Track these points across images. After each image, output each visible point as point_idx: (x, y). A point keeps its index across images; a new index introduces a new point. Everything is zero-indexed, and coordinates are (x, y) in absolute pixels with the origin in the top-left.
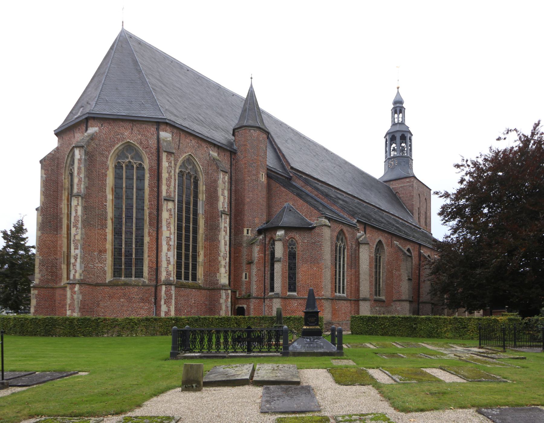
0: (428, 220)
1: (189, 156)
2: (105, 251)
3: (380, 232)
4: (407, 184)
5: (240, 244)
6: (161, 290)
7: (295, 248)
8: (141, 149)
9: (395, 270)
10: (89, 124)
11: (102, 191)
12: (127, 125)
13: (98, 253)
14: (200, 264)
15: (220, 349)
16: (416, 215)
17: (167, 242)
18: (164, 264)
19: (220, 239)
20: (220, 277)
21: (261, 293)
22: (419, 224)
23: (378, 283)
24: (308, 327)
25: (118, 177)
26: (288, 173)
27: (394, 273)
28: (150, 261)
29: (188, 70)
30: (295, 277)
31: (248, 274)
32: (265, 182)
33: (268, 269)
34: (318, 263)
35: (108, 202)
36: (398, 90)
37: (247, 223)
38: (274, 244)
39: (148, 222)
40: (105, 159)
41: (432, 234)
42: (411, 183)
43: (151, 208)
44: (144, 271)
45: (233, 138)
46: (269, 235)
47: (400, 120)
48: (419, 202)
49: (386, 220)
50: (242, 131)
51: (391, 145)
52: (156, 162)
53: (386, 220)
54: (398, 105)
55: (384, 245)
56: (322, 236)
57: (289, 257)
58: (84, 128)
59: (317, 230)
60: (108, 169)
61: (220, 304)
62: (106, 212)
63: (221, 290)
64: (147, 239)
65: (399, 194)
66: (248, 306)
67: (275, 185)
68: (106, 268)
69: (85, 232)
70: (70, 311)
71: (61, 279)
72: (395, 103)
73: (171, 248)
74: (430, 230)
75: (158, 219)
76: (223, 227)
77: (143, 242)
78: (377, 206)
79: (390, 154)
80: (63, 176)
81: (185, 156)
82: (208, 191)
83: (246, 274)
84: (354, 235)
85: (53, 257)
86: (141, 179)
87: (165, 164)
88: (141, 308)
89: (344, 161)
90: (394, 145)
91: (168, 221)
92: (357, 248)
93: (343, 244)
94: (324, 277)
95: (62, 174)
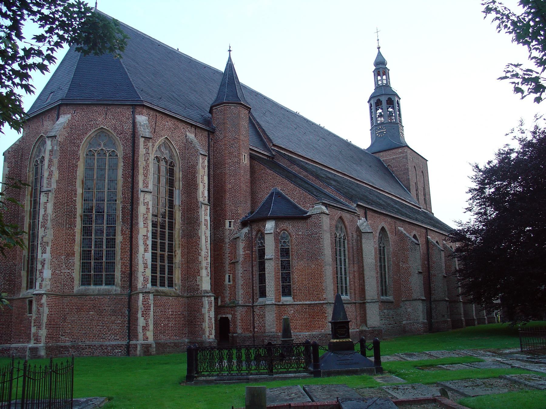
0: (427, 196)
1: (165, 139)
2: (74, 254)
3: (382, 217)
4: (400, 156)
5: (222, 241)
6: (137, 301)
7: (288, 241)
8: (115, 135)
9: (402, 263)
10: (61, 111)
11: (72, 185)
12: (101, 109)
13: (65, 257)
14: (177, 266)
15: (242, 370)
16: (413, 192)
17: (144, 242)
18: (141, 268)
19: (199, 235)
20: (201, 280)
21: (248, 299)
22: (418, 203)
23: (384, 280)
24: (338, 340)
25: (89, 168)
26: (270, 152)
27: (401, 265)
28: (123, 264)
29: (159, 45)
30: (290, 278)
31: (231, 275)
32: (249, 165)
33: (256, 269)
34: (317, 260)
35: (78, 196)
36: (379, 50)
37: (229, 213)
38: (263, 238)
39: (121, 218)
40: (75, 149)
41: (433, 214)
42: (405, 154)
43: (124, 201)
44: (115, 277)
45: (210, 115)
46: (255, 227)
47: (385, 82)
48: (415, 176)
49: (383, 201)
50: (220, 108)
51: (377, 110)
52: (131, 148)
53: (383, 201)
54: (381, 66)
55: (388, 232)
56: (320, 227)
57: (281, 254)
58: (55, 115)
59: (313, 219)
60: (79, 159)
61: (202, 315)
62: (75, 209)
63: (203, 298)
64: (119, 238)
65: (391, 167)
66: (234, 315)
67: (259, 166)
68: (74, 275)
69: (54, 233)
70: (35, 327)
71: (20, 288)
72: (377, 63)
73: (148, 249)
74: (431, 208)
75: (132, 214)
76: (203, 221)
77: (115, 242)
78: (371, 184)
79: (377, 121)
80: (28, 169)
81: (161, 140)
82: (185, 177)
83: (229, 276)
84: (353, 222)
85: (11, 263)
86: (113, 168)
87: (142, 150)
88: (113, 323)
89: (327, 131)
90: (380, 111)
91: (145, 216)
92: (359, 238)
93: (343, 234)
94: (325, 276)
95: (26, 167)
